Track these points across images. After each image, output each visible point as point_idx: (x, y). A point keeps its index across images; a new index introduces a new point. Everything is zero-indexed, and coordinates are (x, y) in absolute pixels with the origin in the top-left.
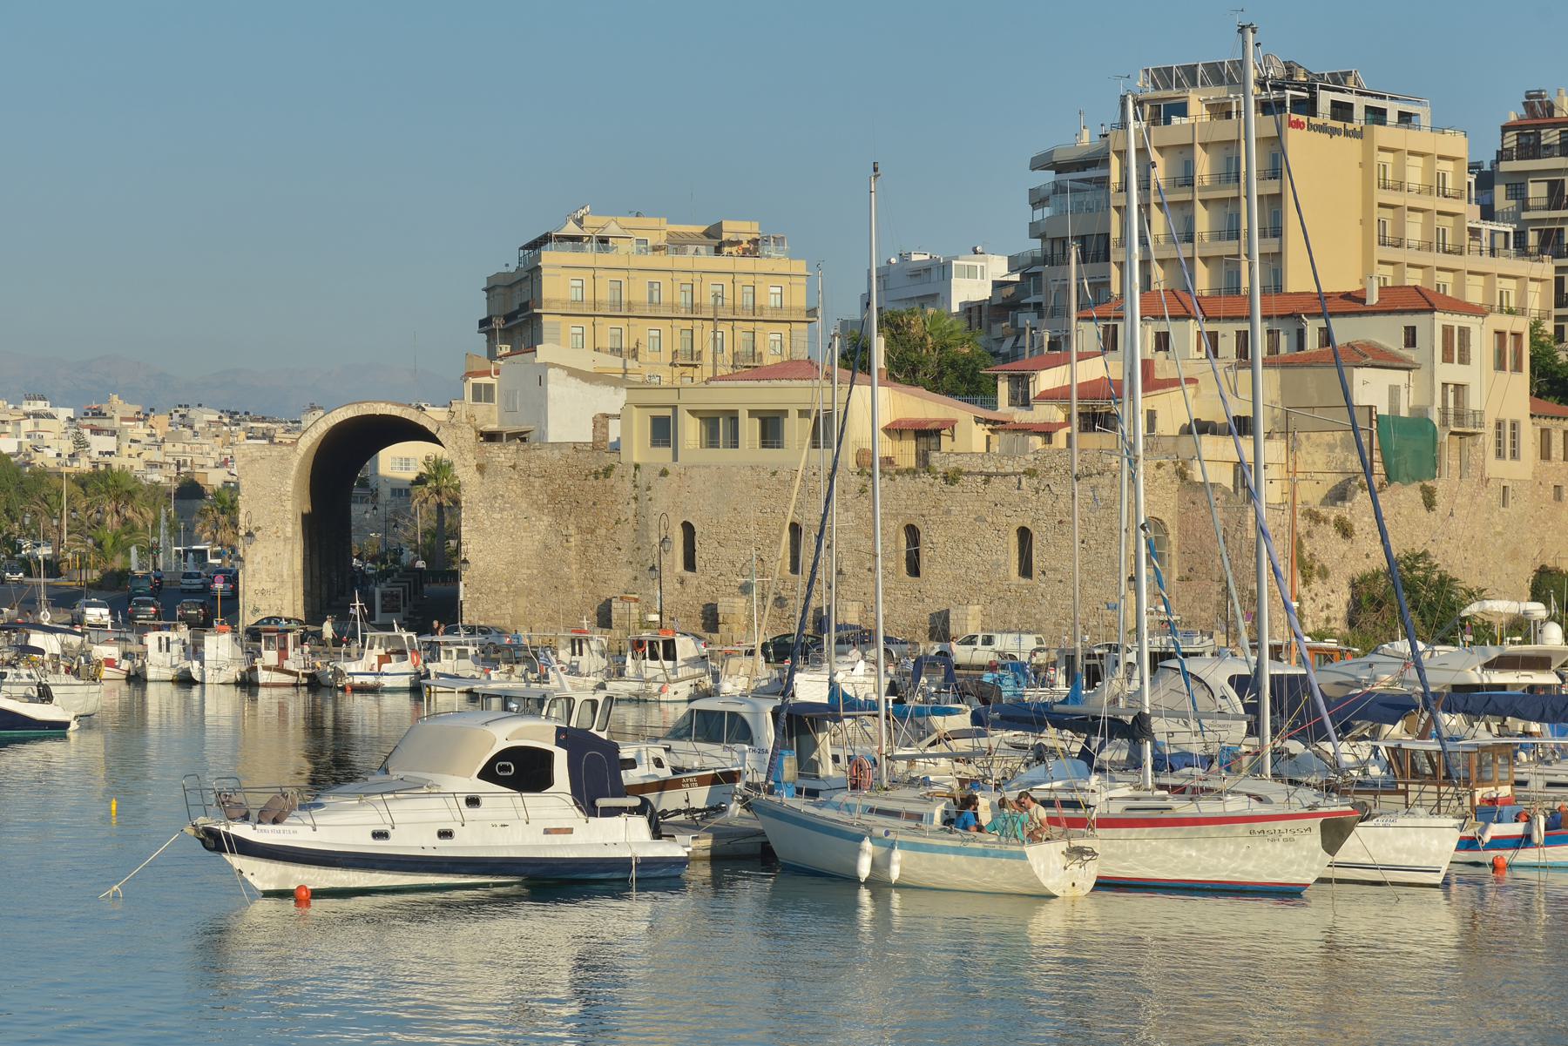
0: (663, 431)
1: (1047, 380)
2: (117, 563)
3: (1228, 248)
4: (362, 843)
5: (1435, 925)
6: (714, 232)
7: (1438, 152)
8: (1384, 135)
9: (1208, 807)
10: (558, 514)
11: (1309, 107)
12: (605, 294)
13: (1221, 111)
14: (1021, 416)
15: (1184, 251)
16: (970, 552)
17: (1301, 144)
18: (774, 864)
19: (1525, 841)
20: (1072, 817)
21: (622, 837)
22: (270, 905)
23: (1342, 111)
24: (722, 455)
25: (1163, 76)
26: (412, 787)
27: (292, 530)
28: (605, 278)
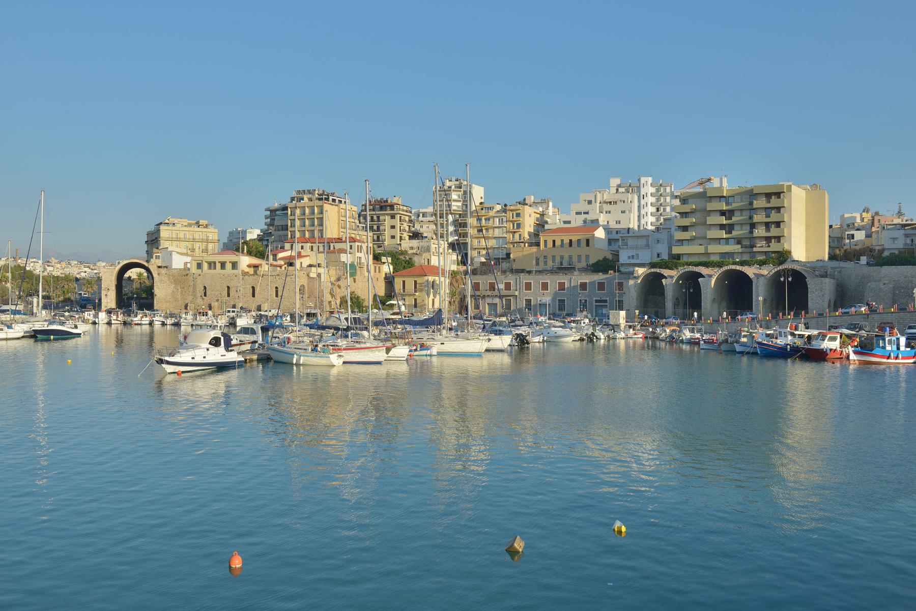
0: (199, 266)
1: (280, 255)
2: (67, 296)
3: (312, 228)
4: (190, 360)
5: (404, 368)
6: (198, 223)
7: (351, 209)
8: (342, 206)
9: (363, 346)
10: (176, 284)
11: (327, 199)
12: (174, 236)
13: (310, 200)
14: (275, 263)
15: (303, 229)
16: (266, 294)
17: (326, 207)
18: (272, 361)
19: (416, 350)
20: (337, 349)
21: (233, 356)
22: (172, 376)
23: (334, 200)
24: (212, 271)
25: (299, 192)
26: (194, 347)
27: (114, 288)
28: (174, 232)
